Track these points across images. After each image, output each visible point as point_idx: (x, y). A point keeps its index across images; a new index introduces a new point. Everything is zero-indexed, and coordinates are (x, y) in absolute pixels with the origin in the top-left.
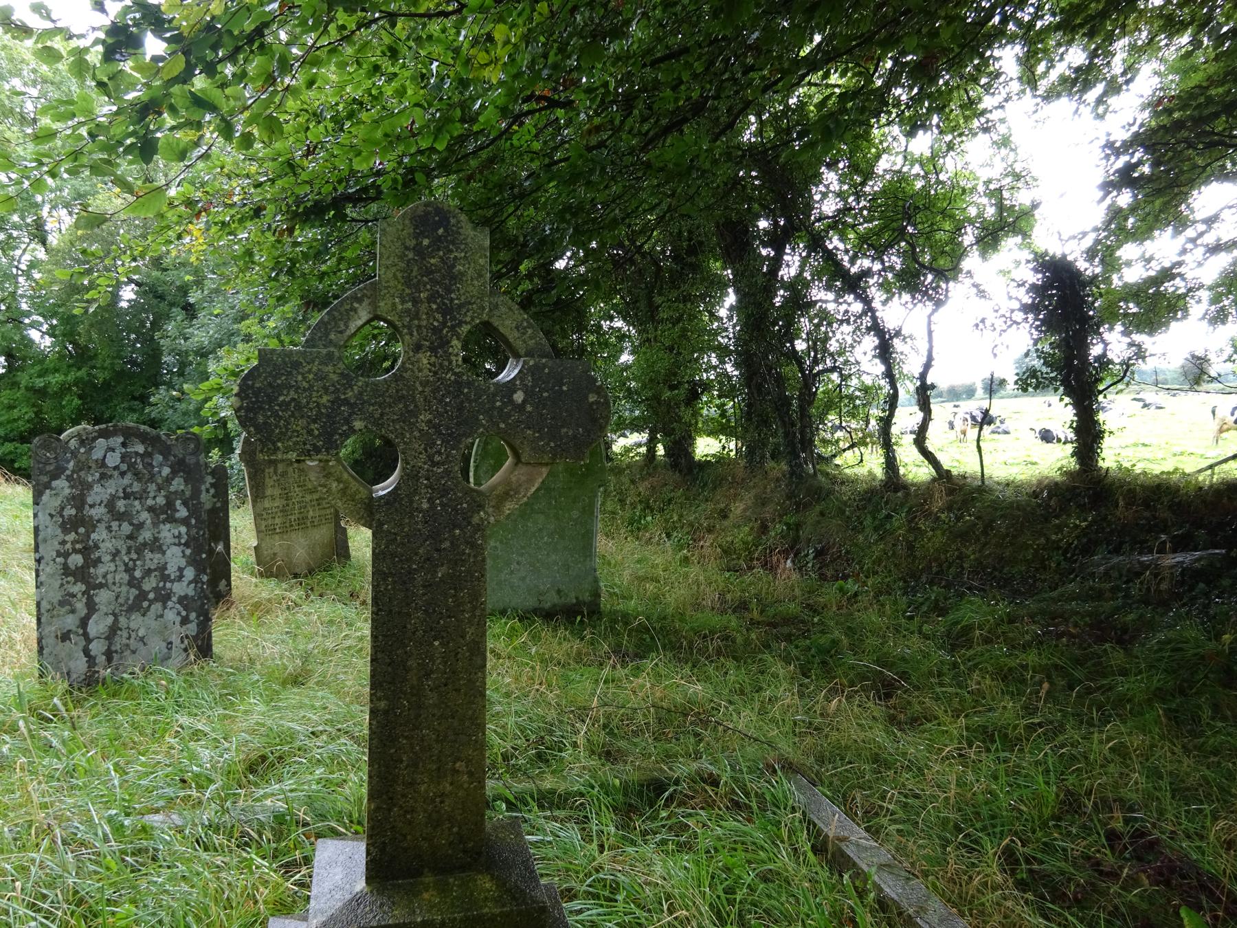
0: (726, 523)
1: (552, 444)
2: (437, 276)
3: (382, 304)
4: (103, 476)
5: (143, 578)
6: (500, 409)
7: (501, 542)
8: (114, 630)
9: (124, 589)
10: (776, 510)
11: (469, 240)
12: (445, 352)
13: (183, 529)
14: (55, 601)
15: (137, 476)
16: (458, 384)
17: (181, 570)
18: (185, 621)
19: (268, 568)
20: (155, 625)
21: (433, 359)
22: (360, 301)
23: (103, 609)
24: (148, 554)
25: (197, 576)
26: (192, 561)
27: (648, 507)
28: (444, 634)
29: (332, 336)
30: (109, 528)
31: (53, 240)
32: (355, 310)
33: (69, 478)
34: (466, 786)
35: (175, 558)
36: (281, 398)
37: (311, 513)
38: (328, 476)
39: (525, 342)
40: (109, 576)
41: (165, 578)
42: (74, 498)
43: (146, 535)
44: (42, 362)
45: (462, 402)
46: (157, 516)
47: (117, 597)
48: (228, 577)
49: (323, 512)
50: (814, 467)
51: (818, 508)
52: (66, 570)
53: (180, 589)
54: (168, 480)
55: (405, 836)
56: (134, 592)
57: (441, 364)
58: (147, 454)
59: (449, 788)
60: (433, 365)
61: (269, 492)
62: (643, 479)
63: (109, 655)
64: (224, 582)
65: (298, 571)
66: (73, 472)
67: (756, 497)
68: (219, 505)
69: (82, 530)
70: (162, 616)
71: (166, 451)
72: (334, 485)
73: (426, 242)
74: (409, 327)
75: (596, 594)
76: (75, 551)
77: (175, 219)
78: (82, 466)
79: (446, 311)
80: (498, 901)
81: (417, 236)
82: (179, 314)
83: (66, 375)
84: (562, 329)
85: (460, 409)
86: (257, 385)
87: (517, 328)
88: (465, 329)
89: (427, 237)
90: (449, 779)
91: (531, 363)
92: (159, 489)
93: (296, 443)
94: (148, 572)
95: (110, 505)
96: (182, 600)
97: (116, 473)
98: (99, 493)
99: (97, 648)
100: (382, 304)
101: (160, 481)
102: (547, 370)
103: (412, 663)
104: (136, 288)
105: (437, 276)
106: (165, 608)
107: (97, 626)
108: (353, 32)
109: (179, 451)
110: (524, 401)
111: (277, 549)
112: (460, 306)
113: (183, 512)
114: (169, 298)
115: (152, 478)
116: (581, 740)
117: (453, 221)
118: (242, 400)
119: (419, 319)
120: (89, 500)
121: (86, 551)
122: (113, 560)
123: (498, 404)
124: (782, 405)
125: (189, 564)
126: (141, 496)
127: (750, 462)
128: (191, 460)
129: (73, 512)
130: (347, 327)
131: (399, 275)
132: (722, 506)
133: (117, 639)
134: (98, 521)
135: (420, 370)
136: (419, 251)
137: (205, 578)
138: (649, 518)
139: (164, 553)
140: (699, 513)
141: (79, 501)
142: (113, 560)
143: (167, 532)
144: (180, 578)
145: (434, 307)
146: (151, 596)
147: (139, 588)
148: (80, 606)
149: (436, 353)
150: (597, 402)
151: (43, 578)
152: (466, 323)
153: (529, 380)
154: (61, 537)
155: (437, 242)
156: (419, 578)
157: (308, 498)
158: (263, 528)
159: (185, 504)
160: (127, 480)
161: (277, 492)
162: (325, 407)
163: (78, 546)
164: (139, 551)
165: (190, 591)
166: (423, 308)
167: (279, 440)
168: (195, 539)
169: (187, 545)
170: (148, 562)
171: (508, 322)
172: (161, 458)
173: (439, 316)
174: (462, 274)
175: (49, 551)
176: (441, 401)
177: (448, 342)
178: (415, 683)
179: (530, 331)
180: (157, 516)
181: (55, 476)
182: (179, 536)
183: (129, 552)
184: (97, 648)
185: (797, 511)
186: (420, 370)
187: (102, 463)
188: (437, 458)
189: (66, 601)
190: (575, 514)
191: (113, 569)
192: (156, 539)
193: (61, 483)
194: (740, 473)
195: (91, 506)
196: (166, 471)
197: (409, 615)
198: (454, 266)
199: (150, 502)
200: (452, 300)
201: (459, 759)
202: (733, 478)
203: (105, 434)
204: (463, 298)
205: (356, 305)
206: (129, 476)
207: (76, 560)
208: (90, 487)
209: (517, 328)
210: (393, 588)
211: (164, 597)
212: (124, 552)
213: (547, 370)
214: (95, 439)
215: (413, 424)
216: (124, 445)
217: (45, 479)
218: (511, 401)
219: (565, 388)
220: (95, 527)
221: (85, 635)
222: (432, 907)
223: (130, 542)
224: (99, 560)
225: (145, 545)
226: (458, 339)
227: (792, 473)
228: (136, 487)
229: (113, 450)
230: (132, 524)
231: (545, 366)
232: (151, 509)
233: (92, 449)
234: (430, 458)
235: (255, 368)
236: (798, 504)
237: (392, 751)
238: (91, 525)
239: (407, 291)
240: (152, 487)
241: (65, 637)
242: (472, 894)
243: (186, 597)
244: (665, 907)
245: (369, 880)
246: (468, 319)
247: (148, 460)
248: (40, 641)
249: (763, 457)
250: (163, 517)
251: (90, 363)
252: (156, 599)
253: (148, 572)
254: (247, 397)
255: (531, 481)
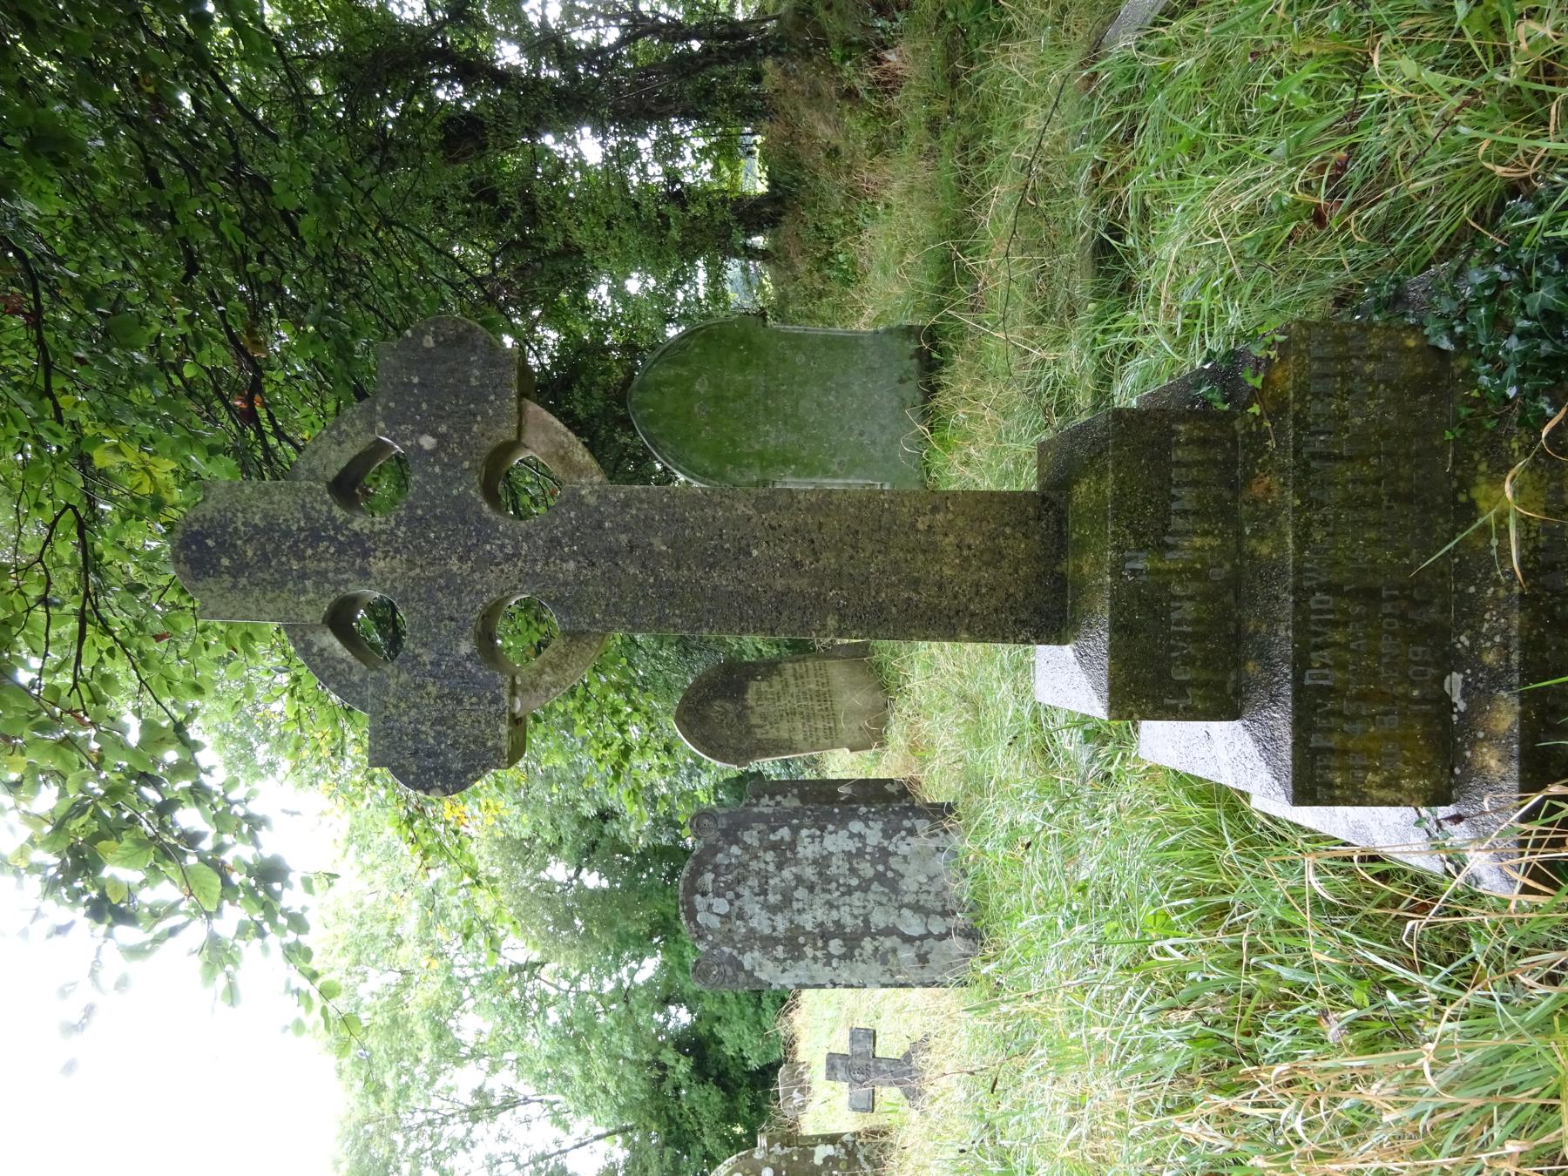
0: (843, 149)
1: (492, 397)
2: (269, 548)
3: (308, 618)
4: (740, 917)
5: (859, 877)
6: (444, 466)
7: (833, 456)
8: (917, 908)
9: (871, 896)
10: (826, 76)
11: (221, 506)
12: (369, 538)
13: (804, 832)
14: (881, 969)
15: (739, 881)
16: (412, 520)
17: (852, 836)
18: (912, 832)
19: (873, 737)
20: (914, 865)
21: (378, 554)
22: (309, 645)
23: (893, 919)
24: (833, 871)
25: (859, 818)
26: (842, 823)
27: (827, 259)
28: (744, 542)
29: (356, 678)
30: (800, 912)
31: (536, 956)
32: (322, 650)
33: (742, 952)
34: (950, 516)
35: (837, 842)
36: (431, 741)
37: (813, 686)
38: (535, 686)
39: (358, 434)
40: (856, 912)
41: (860, 853)
42: (764, 947)
43: (810, 873)
44: (671, 970)
45: (435, 517)
46: (788, 860)
47: (881, 904)
48: (880, 783)
49: (811, 673)
50: (770, 19)
51: (822, 13)
52: (848, 956)
53: (874, 836)
54: (746, 848)
55: (1009, 596)
56: (875, 886)
57: (385, 544)
58: (716, 869)
59: (951, 538)
60: (386, 554)
61: (785, 735)
62: (791, 267)
63: (945, 914)
64: (888, 787)
65: (881, 704)
66: (734, 947)
67: (809, 106)
68: (795, 791)
69: (801, 940)
70: (905, 857)
71: (712, 850)
72: (547, 678)
73: (225, 562)
74: (338, 583)
75: (910, 332)
76: (825, 947)
77: (429, 836)
78: (729, 938)
79: (315, 536)
80: (1101, 476)
81: (217, 572)
82: (611, 828)
83: (685, 945)
84: (603, 373)
85: (442, 519)
86: (415, 769)
87: (339, 444)
88: (338, 512)
89: (219, 559)
90: (939, 538)
91: (382, 425)
92: (757, 857)
93: (488, 723)
94: (853, 871)
95: (774, 910)
96: (887, 835)
97: (737, 903)
98: (760, 921)
99: (937, 926)
100: (308, 618)
101: (747, 857)
102: (392, 405)
103: (779, 584)
104: (585, 871)
105: (269, 548)
106: (895, 854)
107: (913, 926)
108: (116, 640)
109: (712, 836)
110: (434, 435)
111: (854, 726)
112: (308, 518)
113: (784, 833)
114: (593, 838)
115: (745, 866)
116: (1050, 356)
117: (196, 527)
118: (433, 787)
119: (326, 572)
120: (767, 931)
121: (826, 936)
122: (838, 908)
123: (437, 469)
124: (682, 67)
125: (845, 827)
126: (764, 877)
127: (763, 113)
128: (723, 823)
129: (780, 948)
130: (343, 660)
131: (270, 595)
132: (822, 155)
133: (929, 905)
134: (792, 922)
135: (393, 570)
136: (236, 571)
137: (863, 809)
138: (841, 258)
139: (831, 854)
140: (832, 188)
141: (768, 942)
142: (838, 908)
143: (807, 850)
144: (860, 836)
145: (309, 552)
146: (881, 868)
147: (870, 881)
148: (888, 943)
149: (370, 550)
150: (435, 335)
151: (854, 981)
152: (330, 511)
153: (406, 428)
154: (808, 961)
155: (226, 547)
156: (667, 574)
157: (793, 689)
158: (828, 742)
159: (774, 830)
160: (746, 892)
161: (785, 725)
162: (442, 687)
163: (820, 943)
164: (829, 880)
165: (878, 826)
166: (311, 565)
167: (484, 745)
168: (817, 819)
169: (823, 829)
170: (841, 871)
171: (333, 455)
172: (720, 856)
173: (322, 546)
174: (265, 516)
175: (824, 974)
176: (433, 544)
177: (356, 534)
178: (806, 581)
179: (344, 427)
180: (788, 860)
181: (739, 966)
182: (812, 837)
183: (829, 891)
184: (937, 926)
185: (827, 44)
186: (393, 570)
187: (726, 917)
188: (509, 550)
189: (881, 957)
190: (800, 359)
191: (847, 908)
192: (815, 862)
193: (747, 961)
194: (779, 129)
195: (774, 930)
196: (735, 850)
197: (715, 588)
198: (255, 526)
199: (771, 868)
200: (300, 529)
201: (913, 526)
202: (785, 139)
203: (692, 914)
204: (296, 515)
205: (315, 649)
206: (740, 889)
207: (835, 946)
208: (752, 930)
209: (339, 444)
210: (679, 607)
211: (884, 854)
212: (828, 896)
213: (392, 405)
214: (697, 925)
215: (463, 579)
216: (704, 894)
217: (742, 976)
218: (433, 453)
219: (416, 380)
220: (798, 926)
221: (922, 938)
222: (1098, 562)
223: (818, 890)
224: (837, 923)
225: (820, 874)
226: (351, 521)
227: (776, 52)
228: (753, 882)
229: (710, 906)
230: (796, 888)
231: (386, 407)
232: (780, 867)
233: (708, 928)
234: (508, 558)
235: (394, 771)
236: (818, 44)
237: (894, 610)
238: (796, 930)
239: (290, 585)
240: (754, 865)
241: (923, 959)
242: (1090, 510)
243: (884, 831)
244: (1213, 241)
245: (1061, 641)
246: (325, 508)
247: (723, 869)
248: (925, 985)
249: (756, 95)
250: (789, 854)
251: (672, 919)
252: (885, 863)
253: (853, 871)
254: (430, 781)
255: (546, 427)
